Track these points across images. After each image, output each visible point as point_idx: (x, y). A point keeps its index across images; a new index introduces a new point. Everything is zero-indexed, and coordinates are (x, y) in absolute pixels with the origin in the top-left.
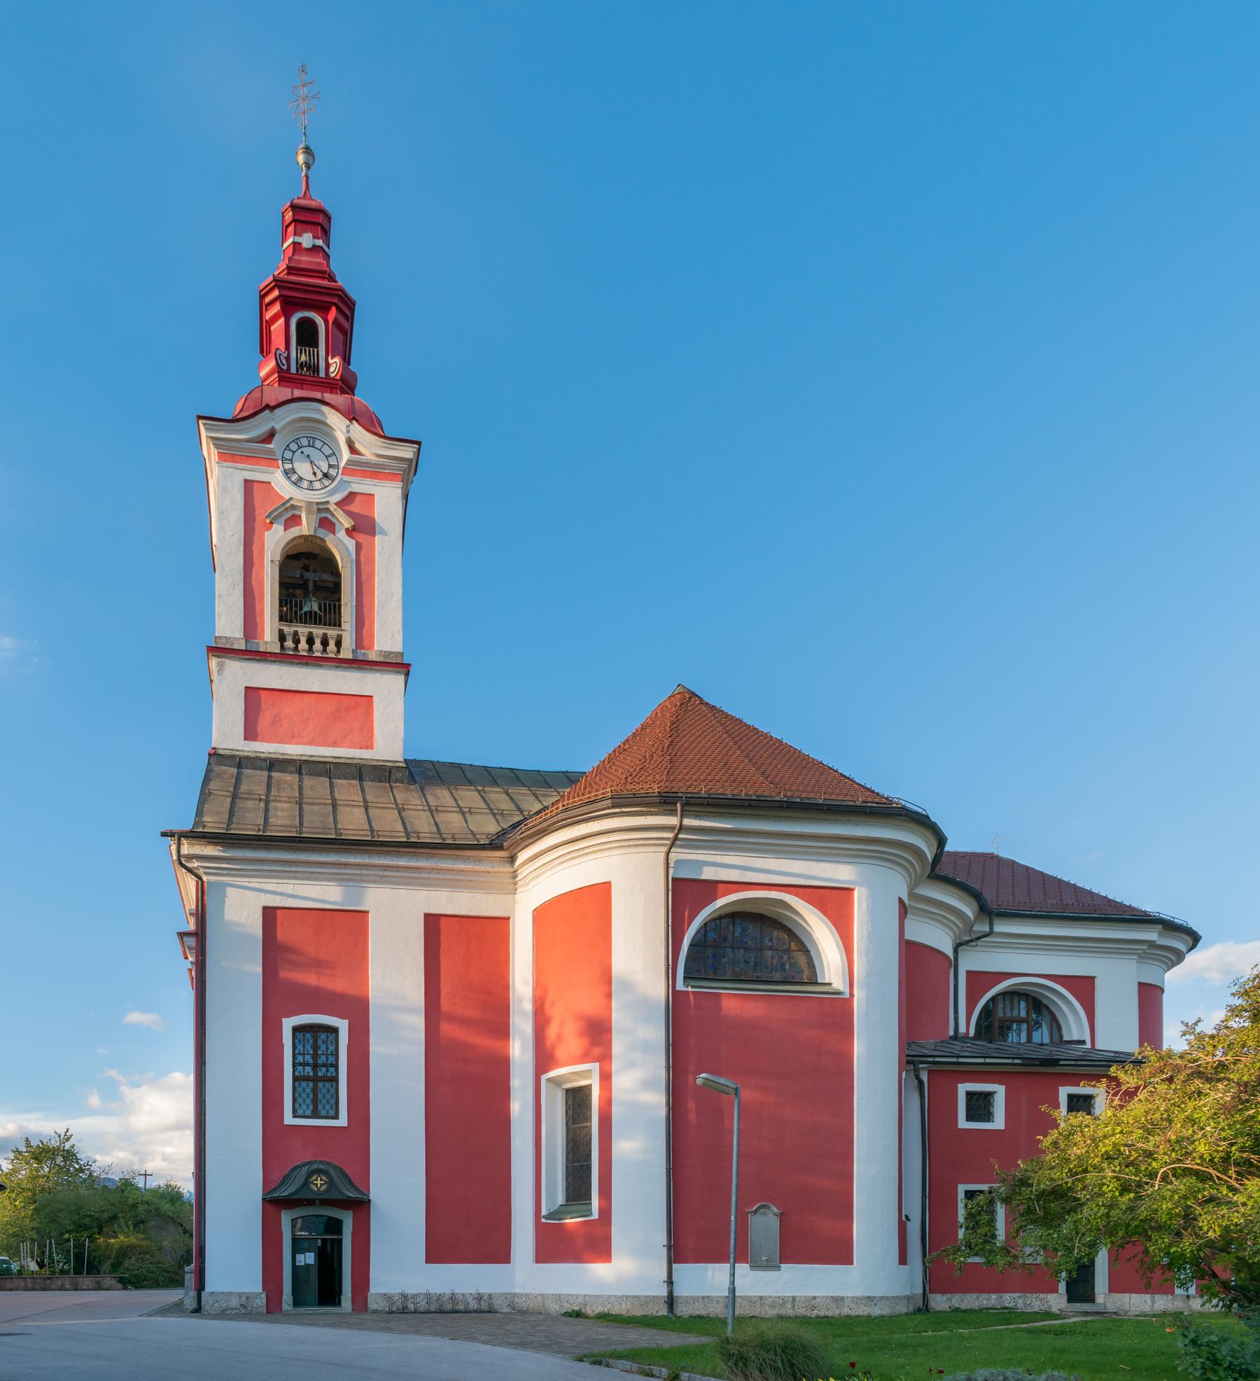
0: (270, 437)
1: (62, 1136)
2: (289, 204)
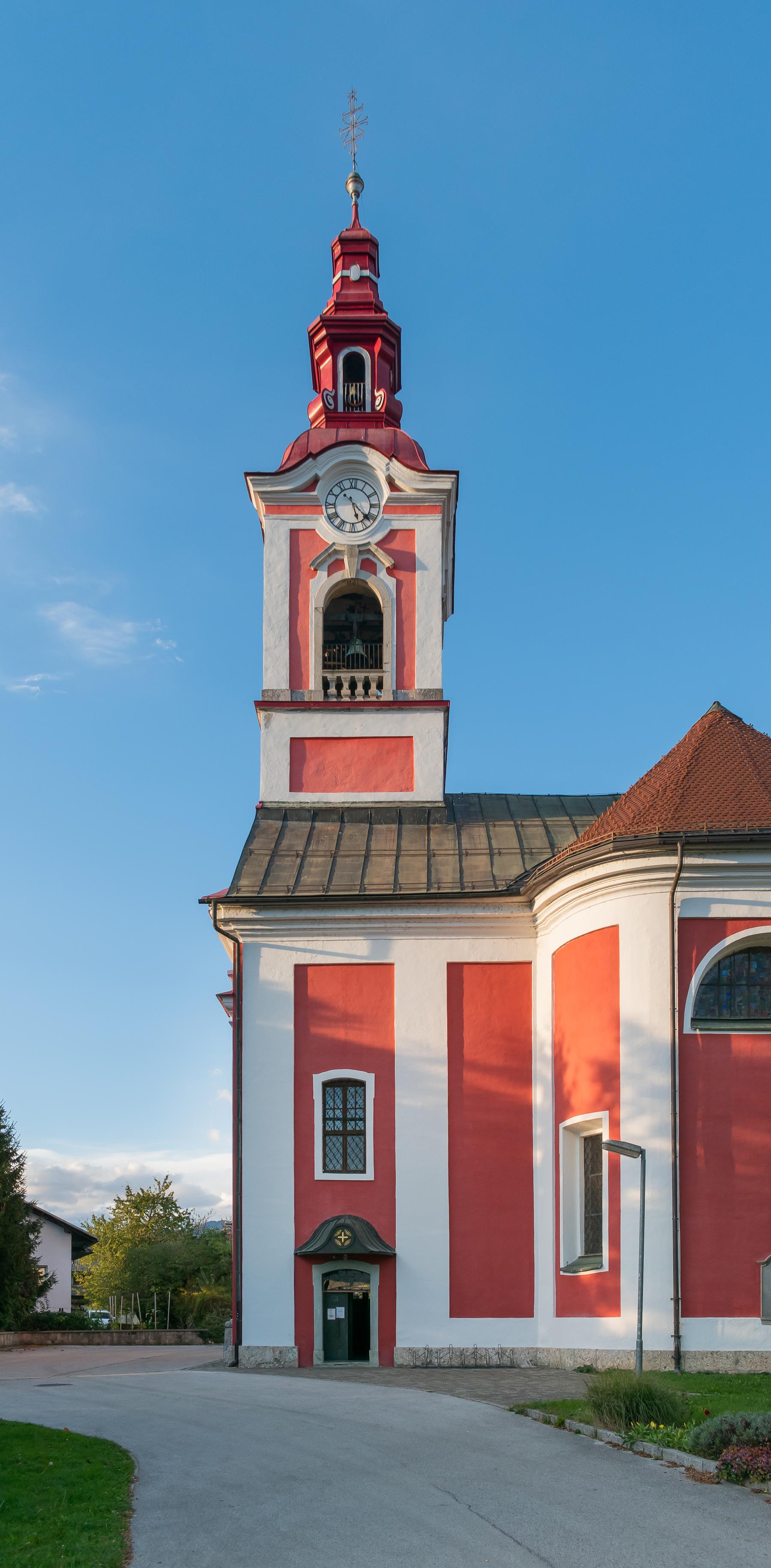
0: (314, 483)
1: (162, 1184)
2: (337, 239)
